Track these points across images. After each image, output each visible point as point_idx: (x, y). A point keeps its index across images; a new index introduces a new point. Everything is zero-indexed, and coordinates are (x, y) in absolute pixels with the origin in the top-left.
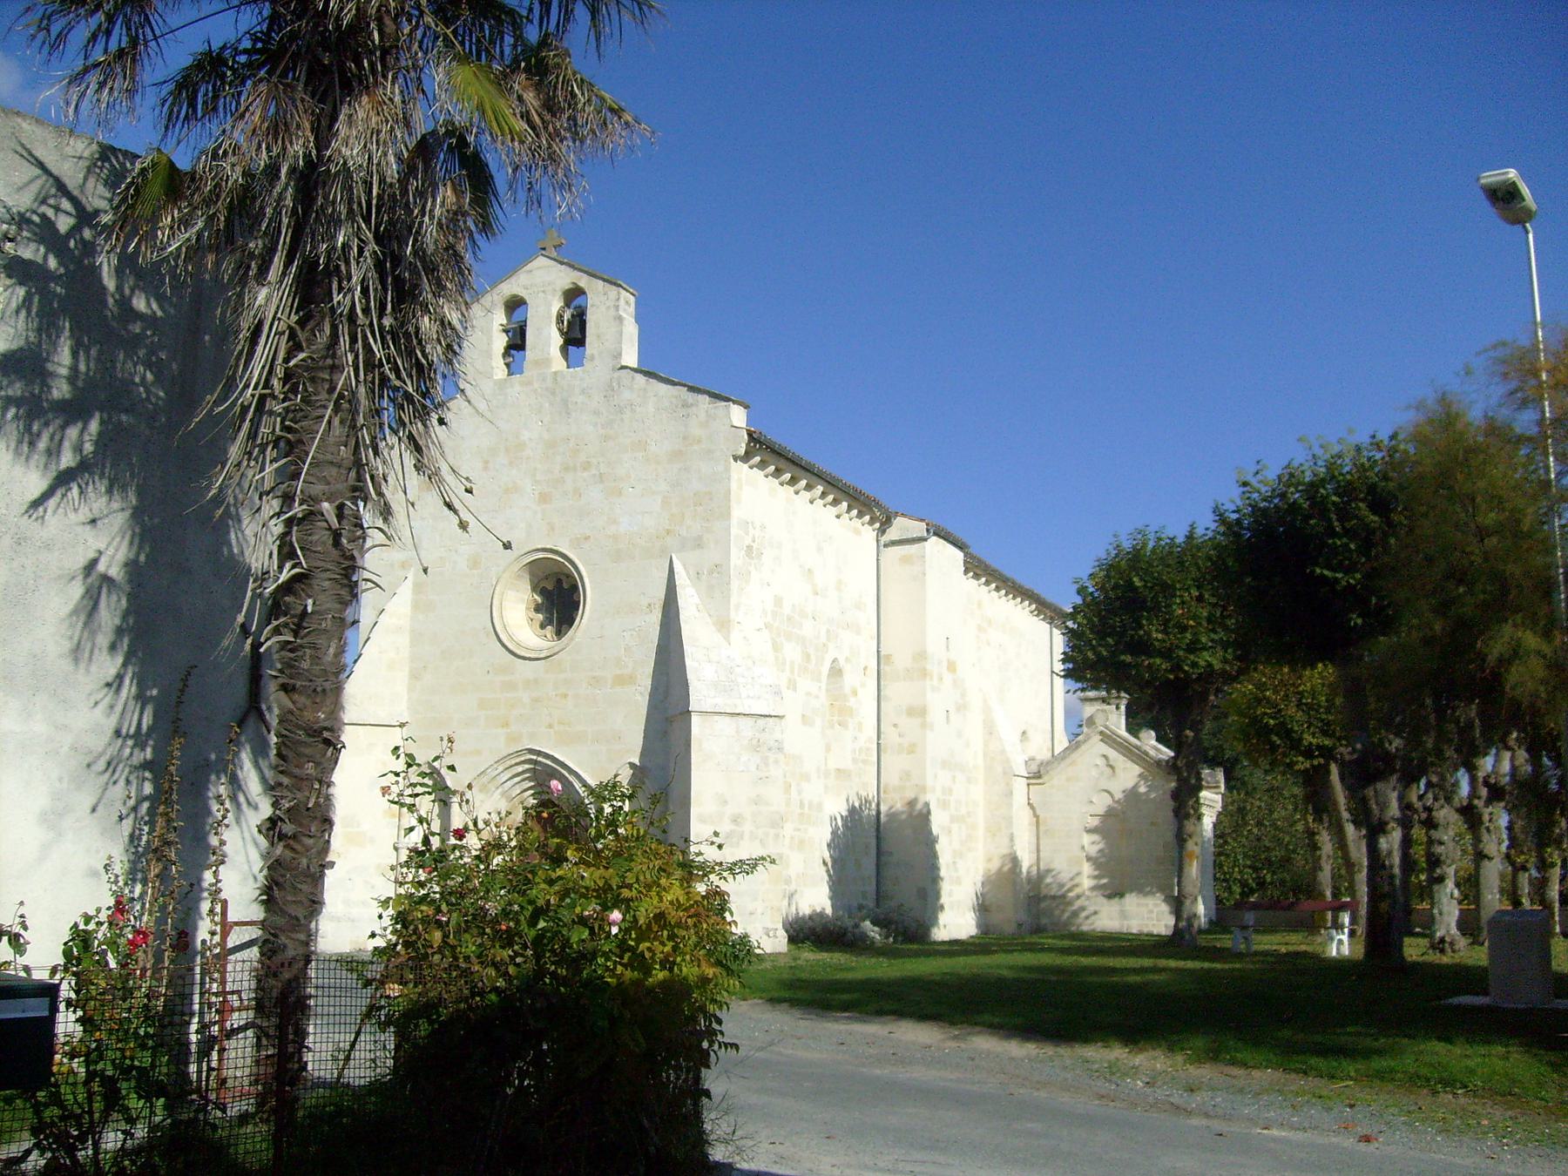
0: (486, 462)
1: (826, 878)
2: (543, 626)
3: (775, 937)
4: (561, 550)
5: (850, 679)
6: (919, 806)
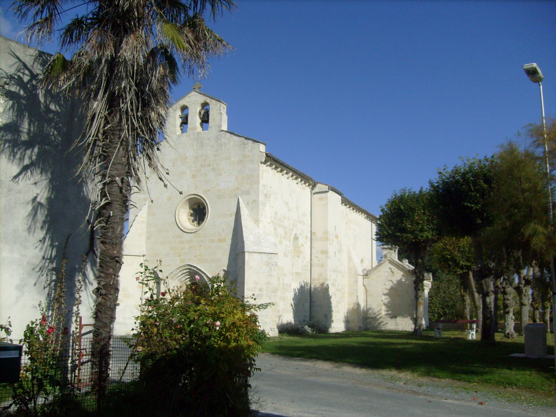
0: (174, 164)
1: (292, 310)
2: (193, 221)
3: (274, 331)
4: (200, 194)
5: (301, 241)
6: (325, 285)
